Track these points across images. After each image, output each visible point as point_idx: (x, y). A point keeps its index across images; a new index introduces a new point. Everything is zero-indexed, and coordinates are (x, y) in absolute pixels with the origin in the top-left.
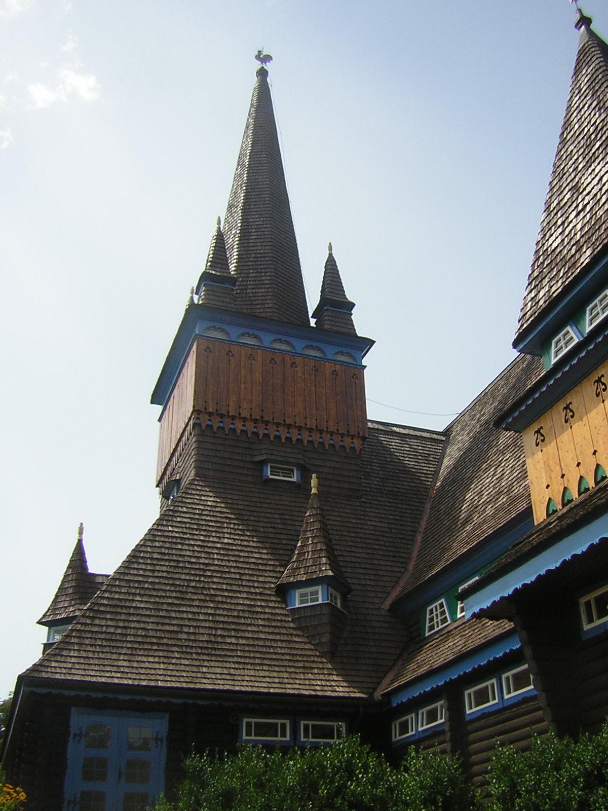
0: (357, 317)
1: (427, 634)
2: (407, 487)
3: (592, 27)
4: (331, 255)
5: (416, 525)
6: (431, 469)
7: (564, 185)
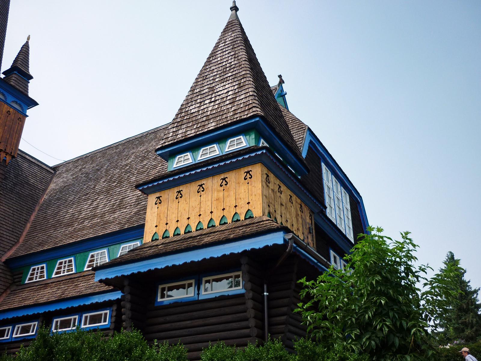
0: (32, 84)
1: (53, 276)
2: (27, 193)
3: (238, 13)
4: (27, 42)
5: (28, 217)
6: (43, 187)
7: (206, 84)
